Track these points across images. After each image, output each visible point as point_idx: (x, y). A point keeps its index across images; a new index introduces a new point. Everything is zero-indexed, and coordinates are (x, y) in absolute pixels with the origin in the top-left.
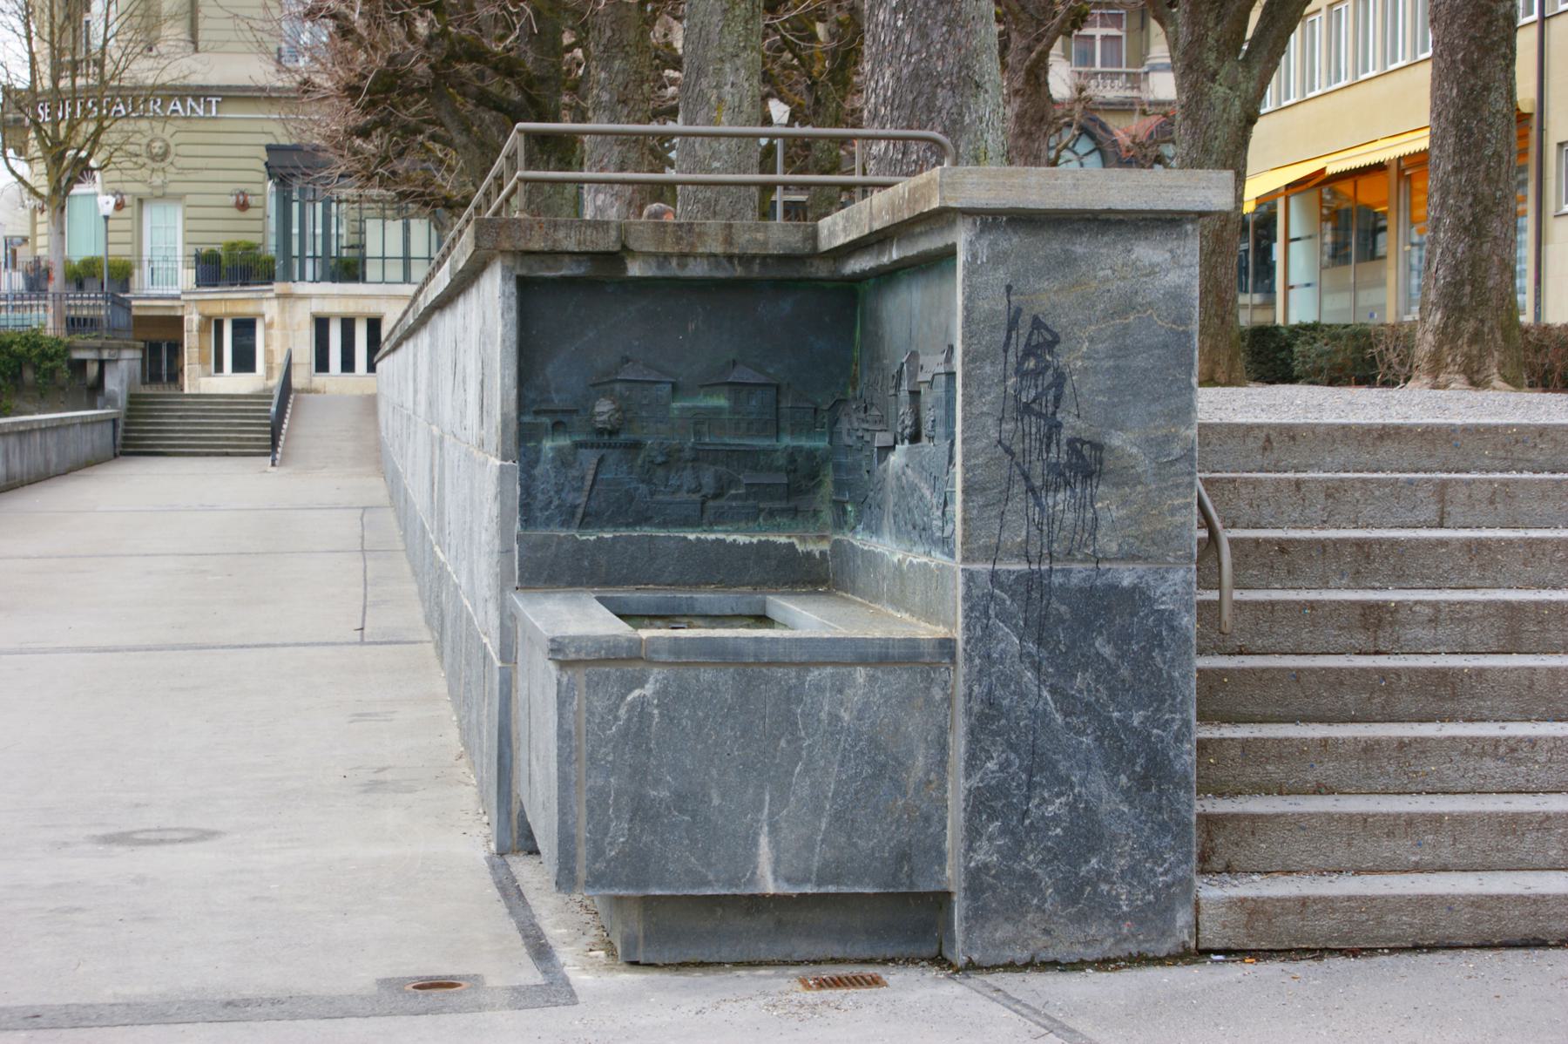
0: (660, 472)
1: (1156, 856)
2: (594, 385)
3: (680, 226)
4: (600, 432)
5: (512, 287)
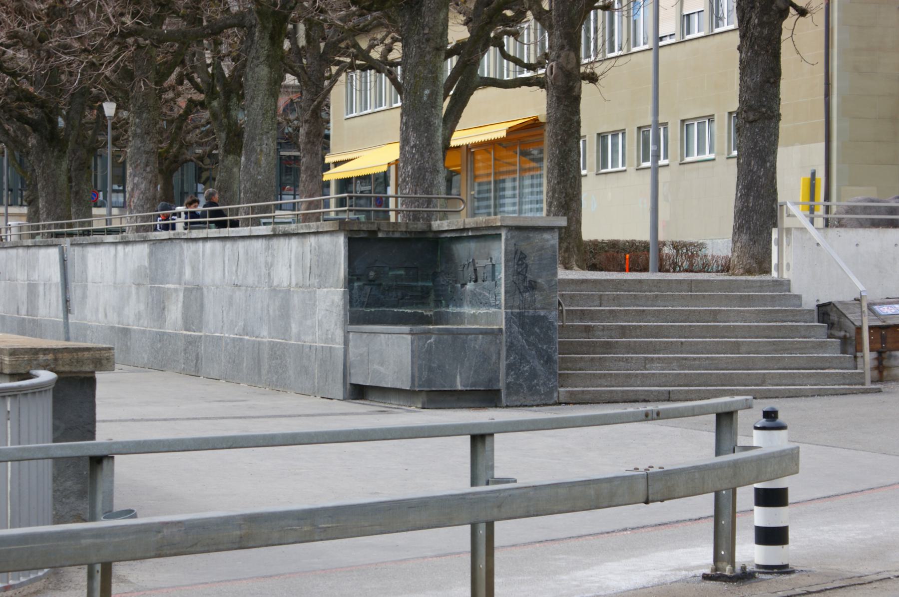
1: (549, 380)
4: (370, 281)
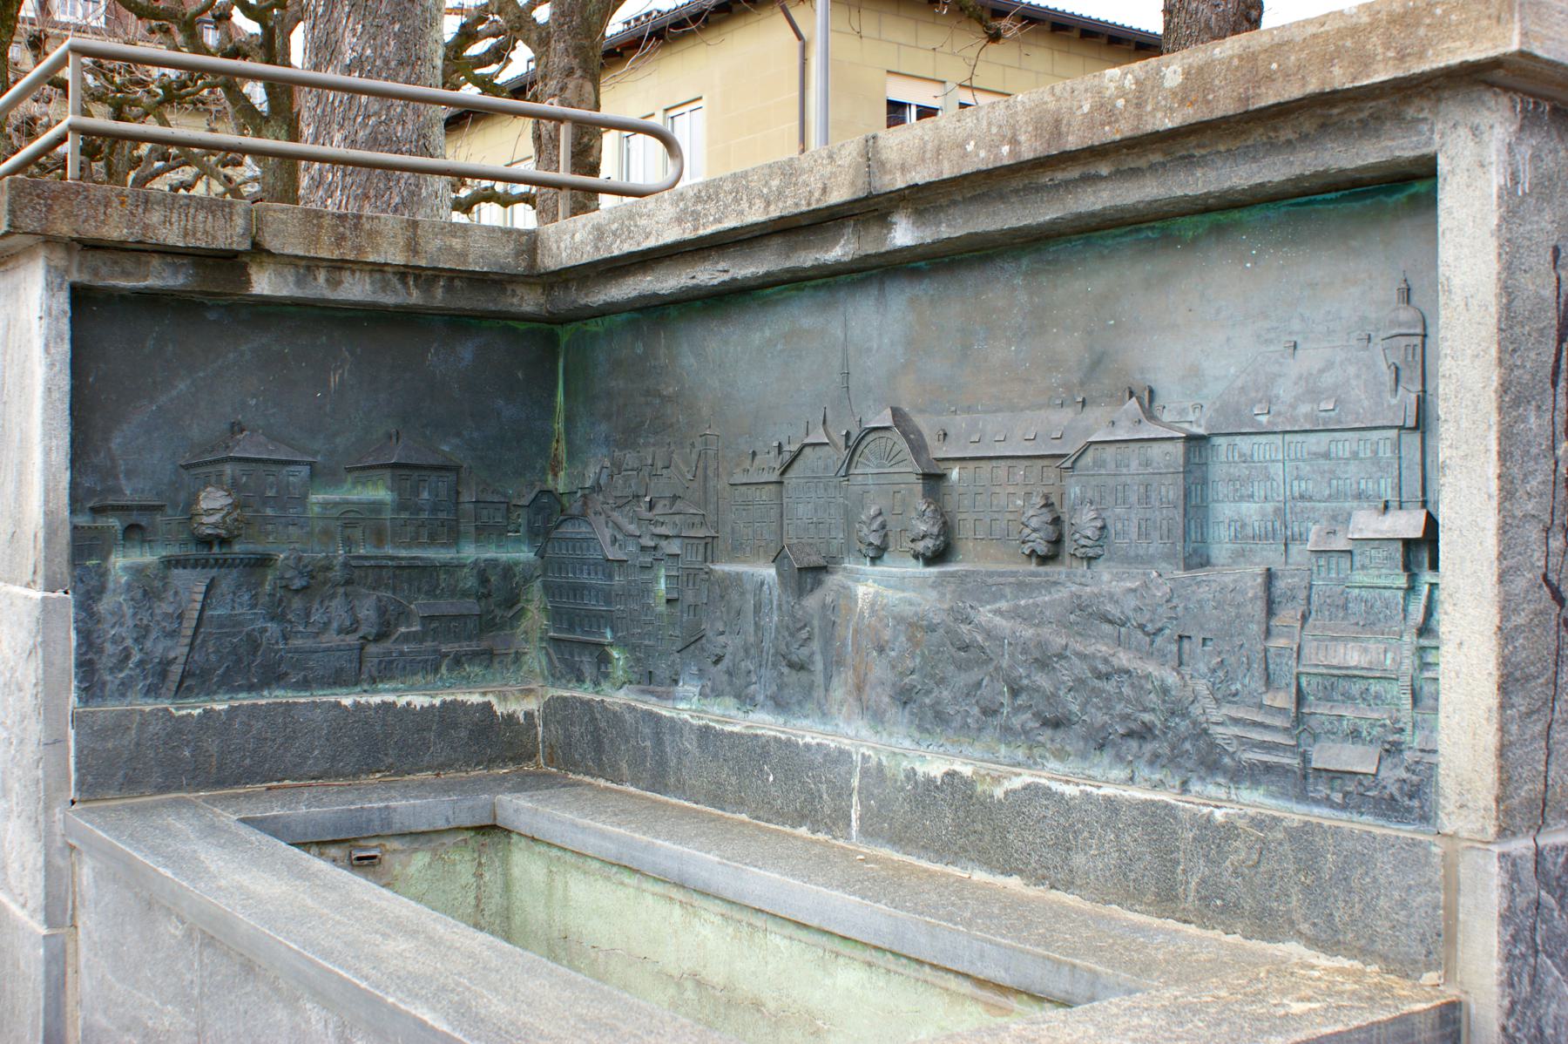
0: (297, 603)
2: (187, 467)
3: (342, 218)
4: (206, 542)
5: (63, 301)
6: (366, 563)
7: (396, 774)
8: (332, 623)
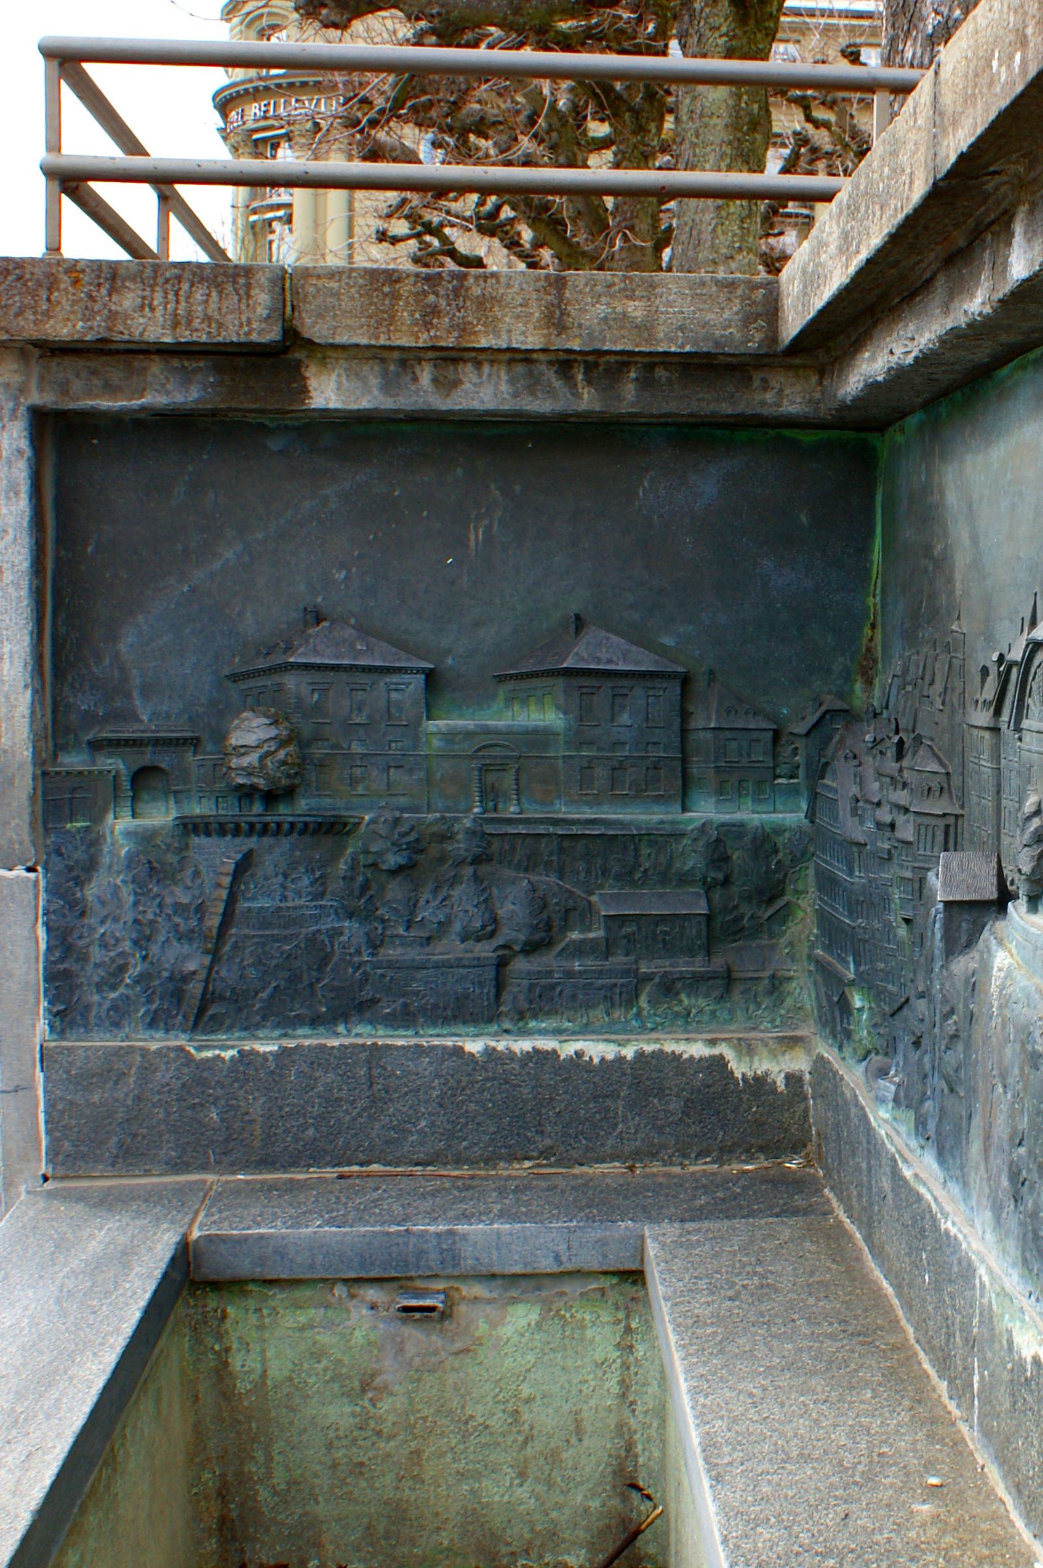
0: (395, 890)
2: (235, 678)
4: (246, 793)
6: (511, 830)
7: (559, 1163)
8: (451, 925)
